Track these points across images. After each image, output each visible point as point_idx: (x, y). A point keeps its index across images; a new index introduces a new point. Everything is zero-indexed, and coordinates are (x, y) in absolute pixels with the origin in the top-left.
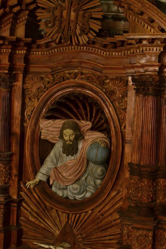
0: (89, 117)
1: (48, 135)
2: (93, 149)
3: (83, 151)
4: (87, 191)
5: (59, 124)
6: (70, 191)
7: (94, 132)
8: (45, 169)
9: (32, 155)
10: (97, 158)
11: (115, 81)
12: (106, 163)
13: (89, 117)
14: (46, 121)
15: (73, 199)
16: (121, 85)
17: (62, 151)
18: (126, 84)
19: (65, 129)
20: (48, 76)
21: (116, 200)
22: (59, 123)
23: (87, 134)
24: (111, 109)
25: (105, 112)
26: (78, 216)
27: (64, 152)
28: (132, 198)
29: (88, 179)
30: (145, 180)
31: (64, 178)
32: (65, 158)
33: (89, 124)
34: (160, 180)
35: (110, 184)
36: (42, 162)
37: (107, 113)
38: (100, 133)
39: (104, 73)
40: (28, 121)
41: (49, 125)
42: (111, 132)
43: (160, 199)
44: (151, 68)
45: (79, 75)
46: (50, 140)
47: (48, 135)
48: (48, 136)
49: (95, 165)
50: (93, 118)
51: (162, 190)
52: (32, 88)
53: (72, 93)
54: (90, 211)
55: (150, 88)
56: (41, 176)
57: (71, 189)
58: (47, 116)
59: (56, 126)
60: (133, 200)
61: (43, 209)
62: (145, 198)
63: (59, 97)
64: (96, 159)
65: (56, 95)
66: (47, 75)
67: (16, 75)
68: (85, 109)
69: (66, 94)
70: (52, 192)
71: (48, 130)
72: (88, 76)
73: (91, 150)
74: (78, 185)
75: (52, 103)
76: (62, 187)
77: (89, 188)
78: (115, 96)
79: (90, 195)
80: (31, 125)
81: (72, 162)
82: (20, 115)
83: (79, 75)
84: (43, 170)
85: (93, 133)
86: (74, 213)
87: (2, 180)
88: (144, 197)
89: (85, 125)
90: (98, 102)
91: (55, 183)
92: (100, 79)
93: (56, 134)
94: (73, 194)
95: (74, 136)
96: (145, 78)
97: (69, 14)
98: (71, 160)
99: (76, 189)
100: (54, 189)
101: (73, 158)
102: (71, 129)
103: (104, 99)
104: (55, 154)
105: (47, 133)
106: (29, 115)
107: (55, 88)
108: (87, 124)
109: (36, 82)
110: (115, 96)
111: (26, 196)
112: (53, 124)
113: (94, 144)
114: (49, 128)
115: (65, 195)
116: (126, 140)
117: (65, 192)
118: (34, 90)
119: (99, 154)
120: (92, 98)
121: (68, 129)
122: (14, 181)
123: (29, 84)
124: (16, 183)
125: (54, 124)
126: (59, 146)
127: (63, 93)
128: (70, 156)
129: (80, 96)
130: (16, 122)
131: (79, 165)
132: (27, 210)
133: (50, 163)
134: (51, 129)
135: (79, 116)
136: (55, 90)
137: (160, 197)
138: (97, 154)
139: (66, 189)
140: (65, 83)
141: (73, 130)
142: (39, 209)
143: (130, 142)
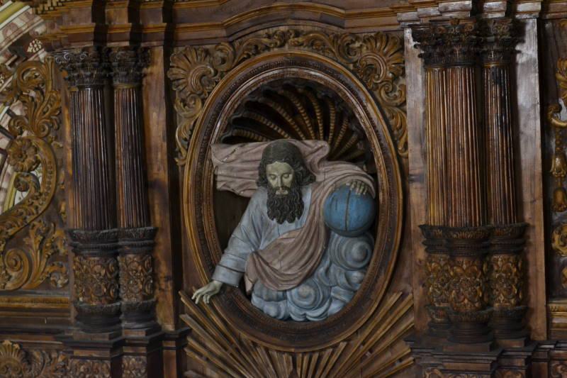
2: (337, 201)
4: (331, 300)
6: (294, 303)
7: (337, 164)
8: (233, 257)
9: (200, 228)
10: (348, 222)
11: (374, 44)
12: (369, 230)
14: (225, 148)
15: (301, 320)
16: (387, 52)
17: (268, 212)
19: (271, 163)
22: (255, 150)
23: (322, 169)
24: (369, 108)
26: (316, 356)
27: (272, 216)
28: (437, 305)
29: (332, 270)
32: (276, 228)
33: (323, 147)
36: (224, 244)
37: (361, 117)
38: (349, 166)
40: (184, 152)
41: (233, 157)
46: (237, 192)
53: (278, 80)
56: (224, 275)
57: (296, 299)
59: (249, 158)
60: (438, 308)
61: (237, 349)
62: (466, 301)
63: (249, 92)
70: (252, 309)
71: (232, 169)
73: (334, 202)
74: (311, 286)
78: (377, 77)
84: (228, 260)
86: (307, 350)
88: (464, 299)
89: (316, 148)
91: (258, 286)
92: (339, 42)
93: (251, 174)
94: (301, 308)
95: (291, 176)
96: (442, 28)
98: (290, 232)
99: (306, 298)
100: (255, 301)
101: (293, 226)
103: (353, 86)
105: (230, 177)
106: (186, 140)
108: (320, 146)
110: (377, 77)
113: (339, 190)
114: (233, 165)
116: (411, 175)
117: (282, 304)
119: (353, 212)
120: (326, 87)
122: (163, 290)
125: (244, 155)
126: (259, 204)
128: (286, 222)
132: (200, 355)
134: (238, 165)
135: (299, 133)
136: (241, 75)
138: (347, 211)
139: (285, 298)
142: (226, 349)
143: (420, 178)
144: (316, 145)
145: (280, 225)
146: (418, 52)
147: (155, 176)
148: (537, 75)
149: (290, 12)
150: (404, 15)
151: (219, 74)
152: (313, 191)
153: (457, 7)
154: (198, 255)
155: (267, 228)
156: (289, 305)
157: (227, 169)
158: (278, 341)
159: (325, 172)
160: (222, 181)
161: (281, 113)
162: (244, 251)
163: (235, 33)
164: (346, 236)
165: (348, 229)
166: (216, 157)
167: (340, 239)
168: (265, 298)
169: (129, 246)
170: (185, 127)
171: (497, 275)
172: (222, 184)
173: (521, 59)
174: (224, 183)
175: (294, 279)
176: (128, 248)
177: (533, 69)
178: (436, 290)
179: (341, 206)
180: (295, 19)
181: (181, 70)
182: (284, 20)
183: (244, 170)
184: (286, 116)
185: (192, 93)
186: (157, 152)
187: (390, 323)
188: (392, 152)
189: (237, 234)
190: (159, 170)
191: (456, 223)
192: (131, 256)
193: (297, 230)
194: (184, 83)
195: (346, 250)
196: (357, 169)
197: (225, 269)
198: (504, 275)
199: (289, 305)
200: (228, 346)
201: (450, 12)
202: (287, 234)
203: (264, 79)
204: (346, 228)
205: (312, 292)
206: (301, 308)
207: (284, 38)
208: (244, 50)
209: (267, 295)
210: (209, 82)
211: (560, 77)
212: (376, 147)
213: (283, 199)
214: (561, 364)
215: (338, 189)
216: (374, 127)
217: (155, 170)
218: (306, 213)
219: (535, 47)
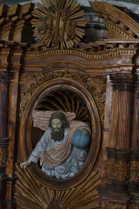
3: (68, 137)
4: (71, 171)
5: (49, 114)
6: (57, 171)
7: (78, 122)
8: (36, 152)
9: (25, 140)
14: (38, 112)
16: (100, 83)
17: (51, 137)
19: (54, 119)
22: (49, 113)
23: (72, 123)
28: (109, 177)
29: (72, 161)
32: (53, 143)
33: (73, 115)
34: (132, 162)
46: (40, 128)
50: (77, 110)
52: (26, 84)
55: (125, 85)
56: (32, 158)
62: (120, 177)
66: (39, 74)
68: (70, 103)
71: (39, 120)
73: (76, 135)
74: (64, 166)
75: (43, 97)
77: (73, 169)
81: (59, 146)
84: (35, 153)
85: (77, 122)
86: (60, 189)
89: (70, 115)
92: (83, 77)
93: (46, 122)
94: (60, 173)
95: (61, 124)
96: (121, 76)
97: (58, 23)
98: (58, 145)
99: (62, 170)
100: (43, 169)
101: (59, 143)
106: (23, 107)
107: (46, 84)
108: (72, 114)
113: (78, 131)
114: (40, 118)
116: (105, 129)
117: (53, 172)
119: (82, 140)
120: (77, 93)
122: (10, 162)
124: (12, 164)
125: (44, 115)
126: (48, 133)
129: (66, 92)
133: (40, 147)
134: (42, 119)
139: (54, 169)
141: (60, 119)
143: (108, 130)
145: (55, 142)
146: (111, 84)
147: (11, 120)
157: (37, 119)
162: (40, 150)
165: (80, 146)
166: (34, 115)
167: (76, 149)
170: (24, 103)
182: (64, 67)
184: (61, 102)
185: (28, 90)
189: (39, 144)
190: (12, 117)
191: (119, 148)
195: (78, 153)
196: (85, 124)
203: (55, 88)
205: (64, 168)
207: (63, 74)
210: (34, 87)
216: (93, 110)
217: (11, 117)
218: (65, 138)
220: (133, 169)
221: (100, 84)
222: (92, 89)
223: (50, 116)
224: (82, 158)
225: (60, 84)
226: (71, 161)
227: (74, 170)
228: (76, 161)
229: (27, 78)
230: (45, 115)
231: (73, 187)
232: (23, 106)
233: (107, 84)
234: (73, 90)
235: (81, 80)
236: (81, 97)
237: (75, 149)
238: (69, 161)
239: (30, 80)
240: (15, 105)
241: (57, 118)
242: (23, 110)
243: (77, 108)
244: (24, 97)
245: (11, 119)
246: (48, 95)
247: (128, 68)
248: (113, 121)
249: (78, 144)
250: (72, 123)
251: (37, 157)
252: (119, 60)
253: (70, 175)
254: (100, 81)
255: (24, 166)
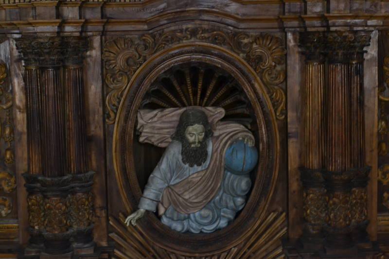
0: (199, 96)
1: (152, 135)
2: (237, 151)
3: (217, 156)
4: (220, 217)
5: (173, 116)
6: (197, 221)
7: (229, 123)
8: (154, 191)
9: (124, 170)
10: (244, 166)
11: (268, 43)
13: (199, 96)
14: (149, 112)
15: (198, 232)
16: (271, 47)
17: (183, 159)
18: (59, 20)
19: (192, 125)
20: (145, 36)
21: (275, 226)
22: (173, 115)
25: (246, 91)
28: (313, 222)
29: (224, 198)
30: (339, 193)
31: (189, 203)
32: (188, 170)
33: (220, 112)
34: (354, 189)
35: (263, 203)
36: (144, 183)
37: (248, 91)
38: (237, 125)
39: (241, 29)
41: (155, 119)
42: (258, 121)
43: (356, 218)
44: (340, 21)
45: (200, 32)
46: (155, 144)
47: (152, 135)
48: (152, 137)
49: (235, 176)
50: (206, 98)
51: (358, 205)
52: (115, 59)
54: (233, 248)
55: (340, 53)
56: (148, 204)
57: (198, 219)
58: (146, 104)
59: (166, 120)
60: (315, 225)
62: (341, 220)
63: (163, 71)
64: (243, 168)
65: (160, 68)
66: (143, 35)
67: (88, 39)
68: (194, 84)
69: (176, 64)
70: (163, 226)
71: (153, 128)
72: (216, 35)
73: (235, 152)
74: (209, 209)
75: (152, 81)
76: (182, 216)
77: (224, 212)
78: (264, 64)
79: (226, 223)
80: (120, 121)
81: (199, 175)
82: (100, 106)
83: (200, 32)
84: (150, 193)
85: (227, 125)
86: (208, 254)
87: (85, 219)
88: (340, 219)
90: (233, 75)
92: (236, 38)
93: (168, 132)
94: (200, 224)
95: (203, 134)
96: (331, 37)
98: (198, 172)
100: (165, 221)
101: (200, 168)
102: (201, 123)
103: (245, 70)
104: (170, 166)
105: (151, 133)
106: (114, 105)
107: (157, 56)
108: (219, 111)
109: (122, 48)
110: (264, 64)
111: (120, 239)
112: (162, 116)
113: (234, 141)
114: (154, 125)
115: (185, 229)
116: (290, 133)
117: (185, 223)
118: (120, 62)
119: (244, 158)
121: (196, 125)
122: (99, 217)
123: (110, 52)
124: (103, 220)
125: (164, 117)
126: (174, 152)
127: (171, 63)
128: (195, 166)
129: (200, 68)
130: (94, 119)
131: (212, 179)
133: (160, 181)
134: (158, 125)
135: (183, 97)
137: (356, 214)
138: (245, 159)
139: (189, 217)
140: (174, 48)
141: (202, 124)
144: (216, 111)
145: (191, 168)
146: (297, 49)
147: (92, 133)
148: (377, 68)
149: (198, 14)
150: (289, 23)
151: (142, 58)
152: (212, 141)
153: (341, 24)
154: (124, 190)
155: (181, 170)
156: (191, 222)
157: (151, 127)
158: (183, 248)
159: (220, 130)
160: (144, 136)
161: (219, 94)
162: (161, 187)
163: (155, 28)
164: (236, 174)
165: (244, 170)
166: (142, 118)
167: (232, 177)
168: (175, 219)
169: (80, 187)
170: (114, 96)
171: (354, 201)
172: (144, 138)
173: (367, 57)
174: (146, 137)
175: (200, 206)
176: (78, 188)
177: (374, 64)
178: (313, 212)
179: (240, 155)
180: (201, 20)
181: (112, 54)
182: (193, 20)
183: (162, 128)
184: (217, 97)
185: (120, 71)
186: (94, 115)
187: (268, 233)
188: (273, 117)
190: (96, 128)
191: (332, 168)
192: (80, 194)
193: (202, 171)
194: (115, 63)
195: (237, 185)
196: (241, 127)
197: (149, 200)
198: (359, 201)
199: (191, 223)
200: (146, 253)
201: (336, 26)
202: (196, 174)
203: (176, 62)
204: (243, 170)
205: (211, 214)
206: (200, 224)
207: (194, 33)
208: (162, 41)
209: (178, 217)
210: (135, 63)
211: (386, 68)
212: (259, 112)
213: (197, 150)
214: (383, 254)
215: (235, 143)
216: (259, 99)
217: (93, 128)
219: (376, 49)
220: (357, 203)
221: (271, 50)
222: (257, 61)
223: (176, 118)
224: (244, 191)
225: (187, 53)
226: (221, 199)
227: (227, 214)
228: (231, 198)
229: (118, 47)
230: (165, 119)
231: (234, 247)
232: (114, 103)
233: (289, 49)
234: (214, 64)
235: (231, 44)
236: (232, 76)
237: (230, 177)
238: (219, 201)
239: (124, 49)
240: (100, 103)
241: (199, 123)
242: (113, 111)
243: (208, 94)
244: (114, 85)
245: (93, 131)
246: (165, 76)
247: (343, 22)
248: (312, 119)
249: (241, 168)
250: (217, 128)
251: (155, 201)
252: (318, 4)
253: (220, 224)
254: (270, 43)
255: (132, 221)
